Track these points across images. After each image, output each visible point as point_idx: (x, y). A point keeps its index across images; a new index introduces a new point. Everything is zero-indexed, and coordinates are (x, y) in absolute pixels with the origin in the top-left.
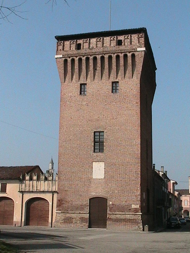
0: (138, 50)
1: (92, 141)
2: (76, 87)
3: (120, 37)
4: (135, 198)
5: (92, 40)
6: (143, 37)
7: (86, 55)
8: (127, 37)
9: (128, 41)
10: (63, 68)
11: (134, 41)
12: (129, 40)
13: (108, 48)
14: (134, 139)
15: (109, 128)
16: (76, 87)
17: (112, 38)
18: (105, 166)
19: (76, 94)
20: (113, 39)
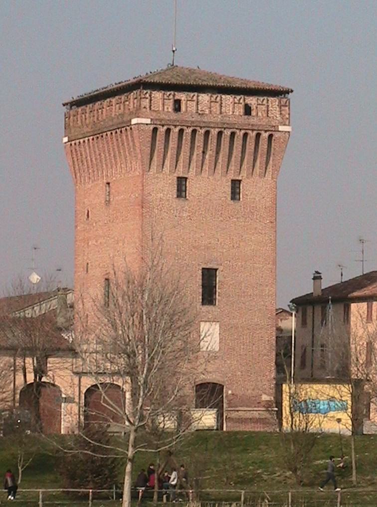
0: (280, 129)
1: (199, 285)
2: (169, 183)
3: (249, 99)
4: (267, 384)
5: (201, 97)
6: (194, 101)
7: (193, 126)
8: (261, 100)
9: (262, 108)
10: (149, 145)
11: (271, 110)
12: (264, 108)
13: (229, 118)
14: (267, 286)
15: (226, 264)
16: (170, 181)
17: (212, 99)
18: (220, 330)
19: (171, 196)
20: (237, 102)
